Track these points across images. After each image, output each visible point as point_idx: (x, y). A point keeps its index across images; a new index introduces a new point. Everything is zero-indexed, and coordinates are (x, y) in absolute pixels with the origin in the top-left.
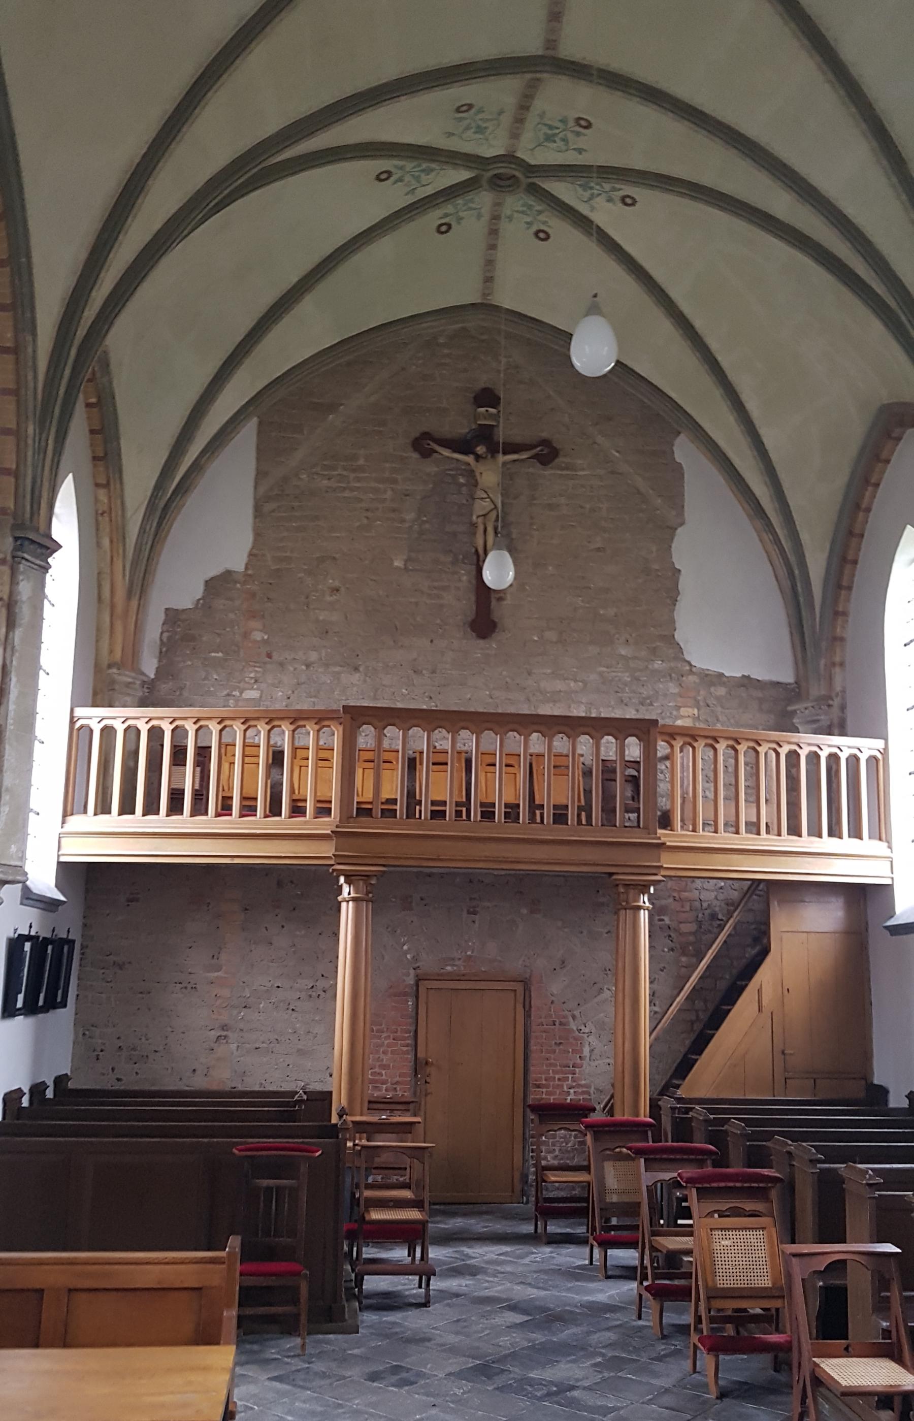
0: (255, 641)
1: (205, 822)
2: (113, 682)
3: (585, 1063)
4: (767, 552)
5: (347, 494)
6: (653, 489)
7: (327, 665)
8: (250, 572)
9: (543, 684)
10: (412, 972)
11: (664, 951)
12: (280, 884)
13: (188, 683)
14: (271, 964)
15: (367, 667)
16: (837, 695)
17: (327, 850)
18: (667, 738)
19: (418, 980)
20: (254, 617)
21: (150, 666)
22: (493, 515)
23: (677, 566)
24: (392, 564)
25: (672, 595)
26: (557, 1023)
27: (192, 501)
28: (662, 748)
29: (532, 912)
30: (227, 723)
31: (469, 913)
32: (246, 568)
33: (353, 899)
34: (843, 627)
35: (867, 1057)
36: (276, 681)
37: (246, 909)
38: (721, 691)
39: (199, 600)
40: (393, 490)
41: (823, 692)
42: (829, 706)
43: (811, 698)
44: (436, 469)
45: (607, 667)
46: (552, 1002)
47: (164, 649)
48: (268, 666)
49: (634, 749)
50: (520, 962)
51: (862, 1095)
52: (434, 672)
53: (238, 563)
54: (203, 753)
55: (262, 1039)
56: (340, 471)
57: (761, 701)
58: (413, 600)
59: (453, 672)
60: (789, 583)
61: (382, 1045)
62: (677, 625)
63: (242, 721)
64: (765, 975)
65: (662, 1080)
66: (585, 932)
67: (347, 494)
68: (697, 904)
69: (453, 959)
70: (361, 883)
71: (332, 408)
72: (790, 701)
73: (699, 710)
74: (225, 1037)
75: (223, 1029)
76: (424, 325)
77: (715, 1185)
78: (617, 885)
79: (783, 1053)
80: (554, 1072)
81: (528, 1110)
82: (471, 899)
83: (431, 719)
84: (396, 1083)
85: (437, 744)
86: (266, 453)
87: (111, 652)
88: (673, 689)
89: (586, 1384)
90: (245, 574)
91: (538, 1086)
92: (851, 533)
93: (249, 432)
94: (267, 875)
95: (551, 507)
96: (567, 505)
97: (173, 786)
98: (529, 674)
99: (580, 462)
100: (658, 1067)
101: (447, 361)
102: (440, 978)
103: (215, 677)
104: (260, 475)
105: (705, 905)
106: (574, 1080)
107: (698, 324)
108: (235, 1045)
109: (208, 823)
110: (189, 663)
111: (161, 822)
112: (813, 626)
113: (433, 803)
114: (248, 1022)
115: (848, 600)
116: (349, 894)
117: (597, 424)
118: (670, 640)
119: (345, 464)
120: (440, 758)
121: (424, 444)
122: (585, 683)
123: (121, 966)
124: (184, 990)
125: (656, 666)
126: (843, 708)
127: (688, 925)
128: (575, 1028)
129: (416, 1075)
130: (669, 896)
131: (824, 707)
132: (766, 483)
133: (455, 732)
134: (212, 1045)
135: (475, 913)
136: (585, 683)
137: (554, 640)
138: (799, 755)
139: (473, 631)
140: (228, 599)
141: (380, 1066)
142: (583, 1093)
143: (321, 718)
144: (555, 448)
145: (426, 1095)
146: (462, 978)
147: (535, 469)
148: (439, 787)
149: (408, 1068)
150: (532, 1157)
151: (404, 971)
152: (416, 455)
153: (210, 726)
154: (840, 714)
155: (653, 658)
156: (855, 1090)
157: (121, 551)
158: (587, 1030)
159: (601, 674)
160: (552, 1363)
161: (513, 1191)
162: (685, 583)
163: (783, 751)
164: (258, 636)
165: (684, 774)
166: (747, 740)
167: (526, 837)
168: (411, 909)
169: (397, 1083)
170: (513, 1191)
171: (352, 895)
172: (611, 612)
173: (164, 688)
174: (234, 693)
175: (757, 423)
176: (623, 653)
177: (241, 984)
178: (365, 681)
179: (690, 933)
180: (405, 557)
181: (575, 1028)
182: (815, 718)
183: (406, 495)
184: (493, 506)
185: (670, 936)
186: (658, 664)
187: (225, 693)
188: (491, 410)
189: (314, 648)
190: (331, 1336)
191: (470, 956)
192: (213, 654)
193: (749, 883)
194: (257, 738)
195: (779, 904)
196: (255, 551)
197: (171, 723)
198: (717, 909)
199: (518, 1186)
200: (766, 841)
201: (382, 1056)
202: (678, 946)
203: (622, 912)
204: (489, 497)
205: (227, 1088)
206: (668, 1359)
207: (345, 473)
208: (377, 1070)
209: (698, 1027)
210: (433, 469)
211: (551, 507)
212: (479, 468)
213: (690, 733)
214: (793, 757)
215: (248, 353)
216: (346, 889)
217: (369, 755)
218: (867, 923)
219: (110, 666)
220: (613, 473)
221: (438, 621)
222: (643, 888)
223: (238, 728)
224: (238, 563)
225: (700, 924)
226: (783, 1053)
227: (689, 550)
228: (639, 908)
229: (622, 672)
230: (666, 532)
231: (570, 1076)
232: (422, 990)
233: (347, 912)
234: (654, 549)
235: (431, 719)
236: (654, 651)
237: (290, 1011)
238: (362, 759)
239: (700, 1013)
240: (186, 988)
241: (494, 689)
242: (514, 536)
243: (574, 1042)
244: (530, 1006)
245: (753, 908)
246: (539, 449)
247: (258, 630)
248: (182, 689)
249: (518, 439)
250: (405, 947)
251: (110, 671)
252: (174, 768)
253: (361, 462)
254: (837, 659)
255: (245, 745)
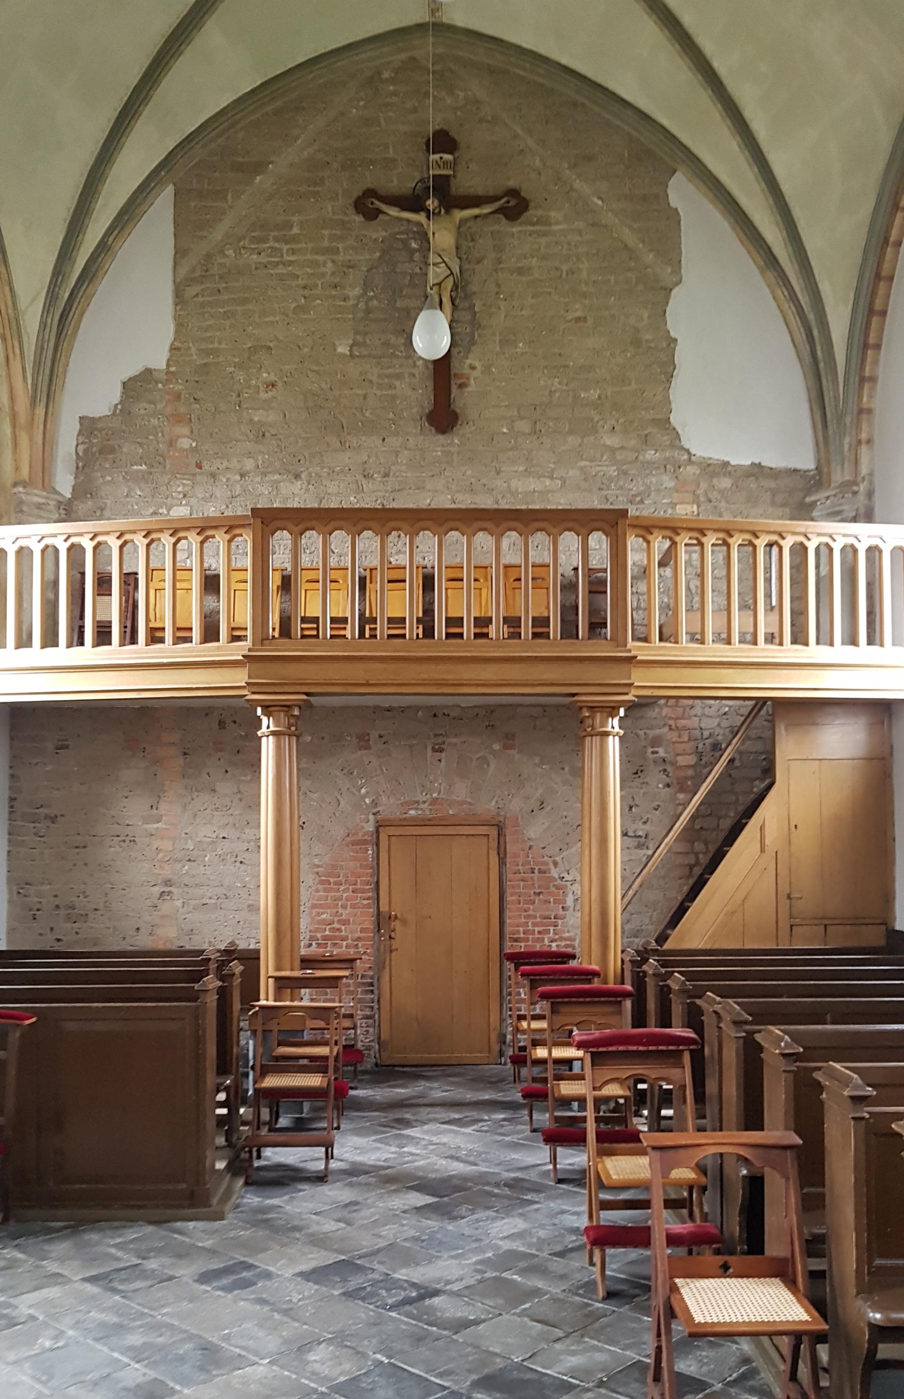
0: (182, 450)
1: (135, 652)
2: (21, 502)
3: (568, 913)
4: (781, 311)
5: (281, 270)
6: (643, 242)
7: (264, 474)
8: (173, 369)
9: (514, 483)
10: (371, 817)
11: (658, 787)
12: (222, 724)
13: (109, 502)
14: (215, 813)
15: (310, 474)
16: (863, 479)
17: (239, 678)
18: (642, 532)
19: (379, 826)
20: (179, 422)
21: (65, 483)
22: (449, 283)
23: (673, 334)
24: (335, 350)
25: (667, 370)
26: (536, 871)
27: (104, 289)
28: (635, 552)
29: (506, 747)
30: (127, 537)
31: (434, 750)
32: (168, 365)
33: (274, 733)
34: (871, 396)
35: (887, 898)
36: (208, 495)
37: (185, 754)
38: (725, 483)
39: (116, 405)
40: (333, 261)
41: (847, 478)
42: (855, 493)
43: (833, 485)
44: (384, 234)
45: (591, 461)
46: (530, 847)
47: (80, 464)
48: (198, 477)
49: (599, 542)
50: (493, 803)
51: (882, 942)
52: (386, 475)
53: (159, 360)
54: (130, 580)
55: (209, 895)
56: (271, 244)
57: (774, 492)
58: (360, 392)
59: (409, 475)
60: (808, 347)
61: (340, 898)
62: (673, 406)
63: (143, 533)
64: (769, 812)
65: (656, 930)
66: (567, 769)
67: (281, 270)
68: (697, 733)
69: (418, 802)
70: (282, 714)
71: (259, 168)
72: (809, 491)
73: (698, 507)
74: (169, 892)
75: (166, 885)
76: (364, 56)
77: (611, 1049)
78: (581, 708)
79: (789, 897)
80: (534, 925)
81: (509, 966)
82: (436, 735)
83: (355, 520)
84: (356, 940)
85: (392, 560)
86: (186, 227)
87: (17, 469)
88: (668, 482)
89: (455, 1287)
90: (168, 373)
91: (516, 940)
92: (878, 276)
93: (164, 202)
94: (207, 715)
95: (521, 271)
96: (539, 267)
97: (98, 618)
98: (498, 473)
99: (553, 214)
100: (651, 917)
101: (394, 99)
102: (404, 823)
103: (139, 493)
104: (180, 253)
105: (706, 734)
106: (556, 934)
107: (687, 19)
108: (181, 901)
109: (140, 652)
110: (109, 478)
111: (88, 653)
112: (836, 398)
113: (391, 620)
114: (194, 876)
115: (876, 362)
116: (268, 727)
117: (575, 165)
118: (665, 424)
119: (276, 233)
120: (395, 575)
121: (367, 205)
122: (563, 480)
123: (53, 819)
124: (122, 844)
125: (648, 457)
126: (870, 494)
127: (687, 757)
128: (557, 877)
129: (379, 930)
130: (665, 725)
131: (849, 495)
132: (777, 224)
133: (384, 534)
134: (156, 901)
135: (441, 751)
136: (563, 480)
137: (527, 431)
138: (806, 549)
139: (431, 424)
140: (150, 402)
141: (339, 921)
142: (566, 946)
143: (231, 527)
144: (524, 199)
145: (391, 951)
146: (428, 823)
147: (502, 225)
148: (401, 603)
149: (369, 924)
150: (510, 1016)
151: (363, 816)
152: (359, 219)
153: (109, 542)
154: (867, 502)
155: (644, 447)
156: (874, 937)
157: (17, 351)
158: (569, 878)
159: (582, 469)
160: (431, 1260)
161: (489, 1052)
162: (682, 354)
163: (787, 544)
164: (185, 443)
165: (651, 577)
166: (741, 531)
167: (469, 654)
168: (368, 748)
169: (359, 939)
170: (489, 1052)
171: (272, 728)
172: (594, 394)
173: (81, 507)
174: (161, 511)
175: (765, 148)
176: (608, 443)
177: (183, 835)
178: (307, 490)
179: (688, 766)
180: (351, 342)
181: (557, 877)
182: (837, 509)
183: (349, 267)
184: (449, 272)
185: (665, 770)
186: (650, 455)
187: (151, 511)
188: (448, 157)
189: (249, 455)
190: (192, 1224)
191: (437, 799)
192: (135, 467)
193: (753, 702)
194: (188, 561)
195: (786, 730)
196: (177, 344)
197: (65, 540)
198: (720, 738)
199: (496, 1047)
200: (764, 652)
201: (340, 910)
202: (675, 782)
203: (588, 739)
204: (444, 261)
205: (174, 947)
206: (573, 1254)
207: (277, 245)
208: (336, 925)
209: (697, 871)
210: (381, 234)
211: (521, 271)
212: (431, 227)
213: (670, 524)
214: (800, 550)
215: (146, 100)
216: (265, 720)
217: (311, 575)
218: (892, 748)
219: (15, 485)
220: (594, 225)
221: (391, 415)
222: (612, 711)
223: (167, 540)
224: (159, 360)
225: (700, 755)
226: (789, 897)
227: (684, 316)
228: (607, 734)
229: (607, 466)
230: (660, 293)
231: (552, 929)
232: (383, 837)
233: (268, 747)
234: (646, 315)
235: (355, 520)
236: (646, 440)
237: (238, 864)
238: (304, 580)
239: (701, 856)
240: (124, 841)
241: (457, 492)
242: (476, 309)
243: (556, 891)
244: (505, 854)
245: (762, 735)
246: (503, 201)
247: (185, 436)
248: (102, 510)
249: (480, 191)
250: (363, 791)
251: (15, 490)
252: (99, 598)
253: (296, 230)
254: (864, 436)
255: (175, 570)
